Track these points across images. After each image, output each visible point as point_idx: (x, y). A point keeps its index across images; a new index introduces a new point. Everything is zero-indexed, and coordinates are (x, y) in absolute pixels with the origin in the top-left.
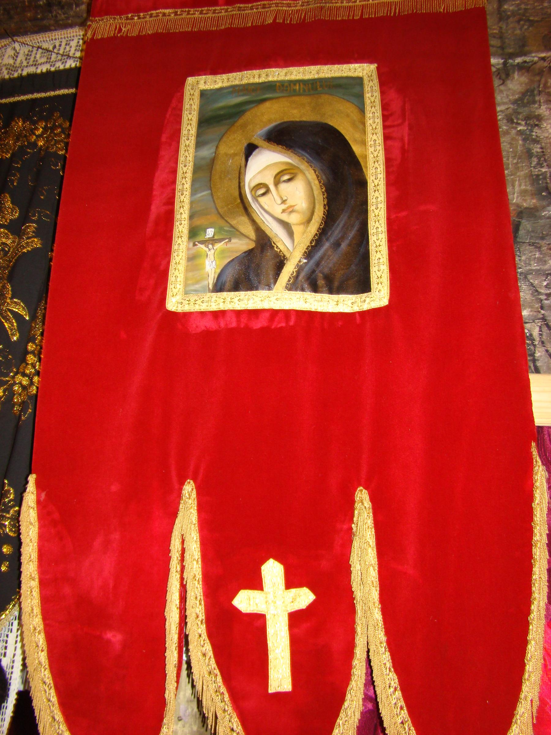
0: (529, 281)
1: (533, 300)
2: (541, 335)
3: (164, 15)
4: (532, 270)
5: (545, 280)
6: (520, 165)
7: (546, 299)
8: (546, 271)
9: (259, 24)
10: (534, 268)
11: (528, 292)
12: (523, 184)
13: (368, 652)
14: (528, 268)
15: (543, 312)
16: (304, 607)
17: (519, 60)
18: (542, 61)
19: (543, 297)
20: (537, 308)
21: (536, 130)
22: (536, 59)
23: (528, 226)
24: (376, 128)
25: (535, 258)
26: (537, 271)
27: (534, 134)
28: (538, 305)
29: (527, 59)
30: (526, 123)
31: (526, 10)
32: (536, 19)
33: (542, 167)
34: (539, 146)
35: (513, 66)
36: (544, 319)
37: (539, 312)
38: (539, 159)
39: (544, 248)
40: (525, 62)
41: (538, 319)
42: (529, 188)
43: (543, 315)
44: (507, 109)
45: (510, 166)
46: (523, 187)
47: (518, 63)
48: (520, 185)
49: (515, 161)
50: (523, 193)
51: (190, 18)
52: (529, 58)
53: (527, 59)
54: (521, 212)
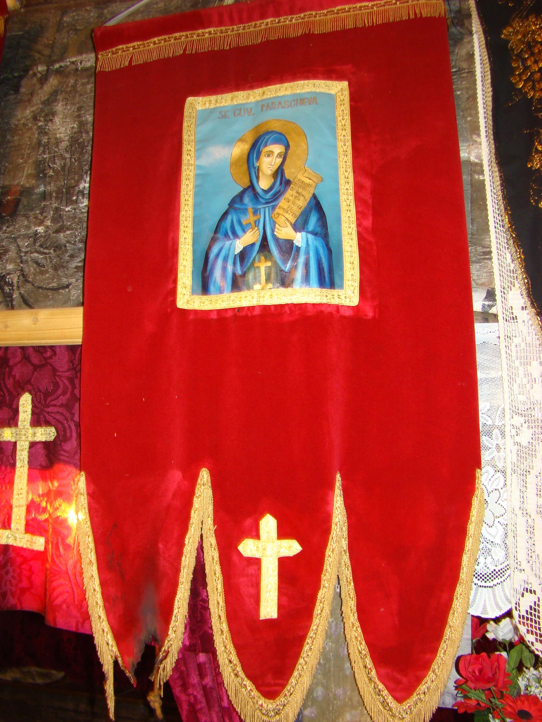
0: (17, 243)
1: (16, 257)
2: (18, 282)
3: (176, 39)
4: (21, 235)
5: (27, 242)
6: (31, 154)
7: (24, 256)
8: (30, 234)
9: (319, 32)
10: (22, 233)
11: (14, 251)
12: (30, 169)
13: (202, 536)
14: (18, 233)
15: (21, 265)
16: (276, 521)
17: (57, 66)
18: (72, 65)
19: (23, 254)
20: (19, 263)
21: (50, 124)
22: (69, 63)
23: (25, 202)
24: (345, 125)
25: (24, 226)
26: (24, 235)
27: (47, 127)
28: (19, 261)
29: (62, 64)
30: (44, 120)
31: (78, 20)
32: (81, 28)
33: (45, 154)
34: (47, 137)
35: (53, 71)
36: (22, 270)
37: (19, 265)
38: (44, 148)
39: (31, 218)
40: (61, 67)
41: (18, 271)
42: (33, 172)
43: (22, 267)
44: (37, 109)
45: (25, 156)
46: (30, 172)
47: (56, 69)
48: (28, 171)
49: (29, 152)
50: (29, 176)
51: (201, 39)
52: (64, 63)
53: (62, 64)
54: (23, 192)
